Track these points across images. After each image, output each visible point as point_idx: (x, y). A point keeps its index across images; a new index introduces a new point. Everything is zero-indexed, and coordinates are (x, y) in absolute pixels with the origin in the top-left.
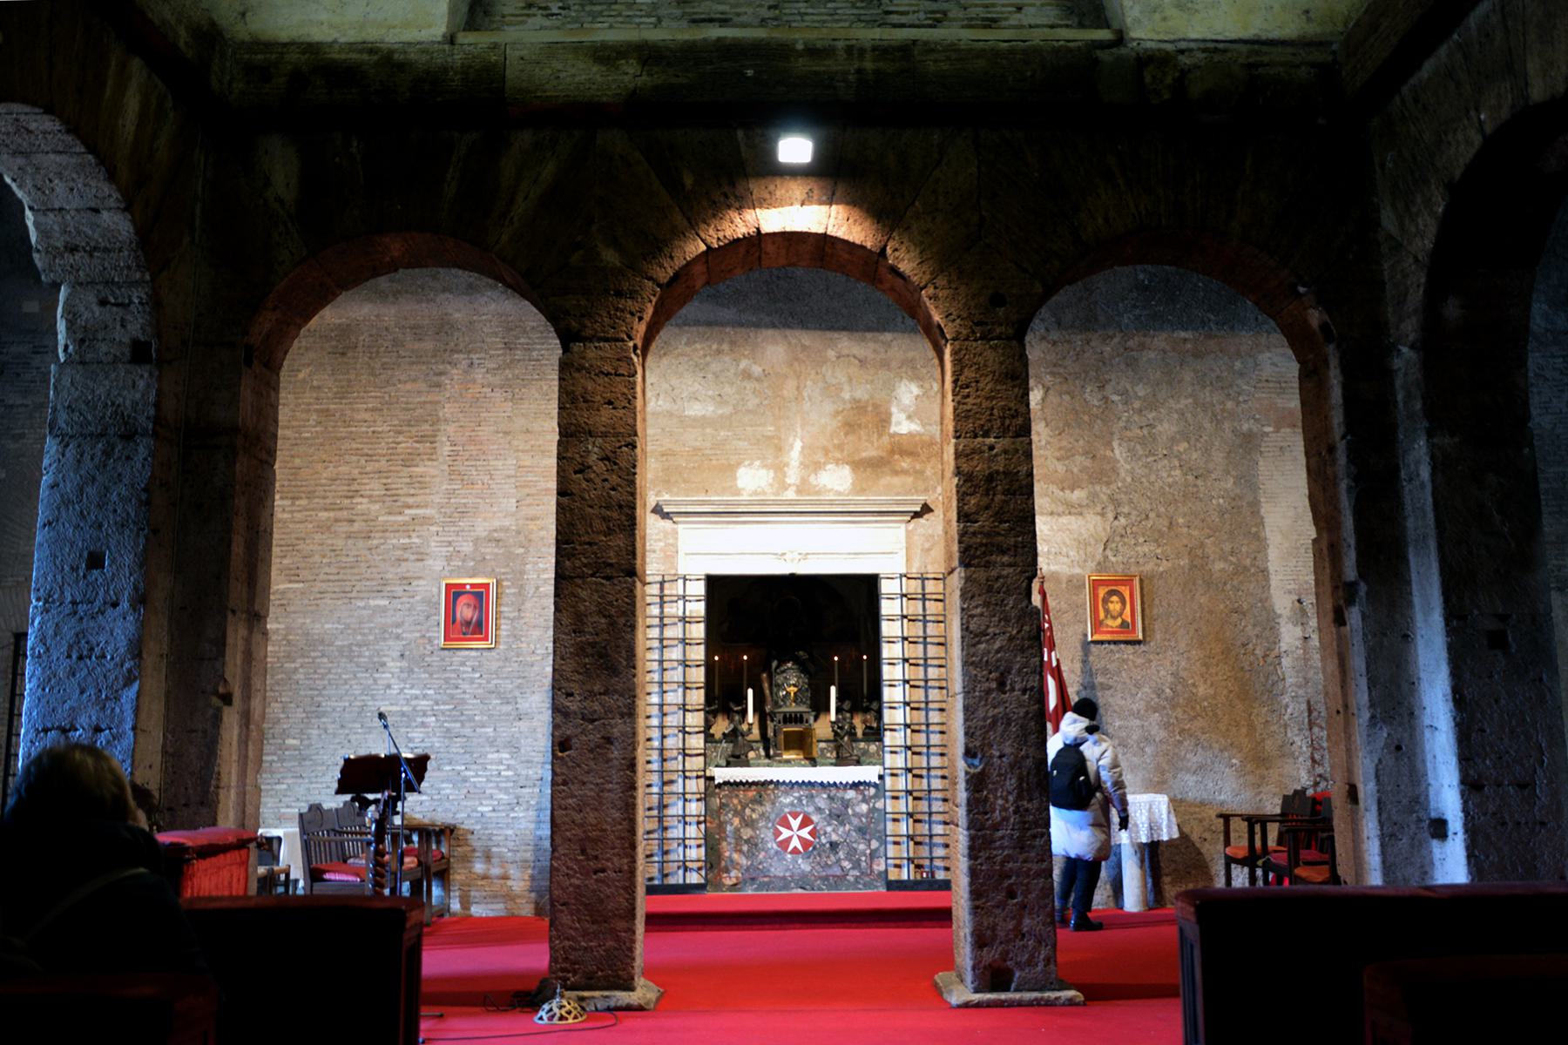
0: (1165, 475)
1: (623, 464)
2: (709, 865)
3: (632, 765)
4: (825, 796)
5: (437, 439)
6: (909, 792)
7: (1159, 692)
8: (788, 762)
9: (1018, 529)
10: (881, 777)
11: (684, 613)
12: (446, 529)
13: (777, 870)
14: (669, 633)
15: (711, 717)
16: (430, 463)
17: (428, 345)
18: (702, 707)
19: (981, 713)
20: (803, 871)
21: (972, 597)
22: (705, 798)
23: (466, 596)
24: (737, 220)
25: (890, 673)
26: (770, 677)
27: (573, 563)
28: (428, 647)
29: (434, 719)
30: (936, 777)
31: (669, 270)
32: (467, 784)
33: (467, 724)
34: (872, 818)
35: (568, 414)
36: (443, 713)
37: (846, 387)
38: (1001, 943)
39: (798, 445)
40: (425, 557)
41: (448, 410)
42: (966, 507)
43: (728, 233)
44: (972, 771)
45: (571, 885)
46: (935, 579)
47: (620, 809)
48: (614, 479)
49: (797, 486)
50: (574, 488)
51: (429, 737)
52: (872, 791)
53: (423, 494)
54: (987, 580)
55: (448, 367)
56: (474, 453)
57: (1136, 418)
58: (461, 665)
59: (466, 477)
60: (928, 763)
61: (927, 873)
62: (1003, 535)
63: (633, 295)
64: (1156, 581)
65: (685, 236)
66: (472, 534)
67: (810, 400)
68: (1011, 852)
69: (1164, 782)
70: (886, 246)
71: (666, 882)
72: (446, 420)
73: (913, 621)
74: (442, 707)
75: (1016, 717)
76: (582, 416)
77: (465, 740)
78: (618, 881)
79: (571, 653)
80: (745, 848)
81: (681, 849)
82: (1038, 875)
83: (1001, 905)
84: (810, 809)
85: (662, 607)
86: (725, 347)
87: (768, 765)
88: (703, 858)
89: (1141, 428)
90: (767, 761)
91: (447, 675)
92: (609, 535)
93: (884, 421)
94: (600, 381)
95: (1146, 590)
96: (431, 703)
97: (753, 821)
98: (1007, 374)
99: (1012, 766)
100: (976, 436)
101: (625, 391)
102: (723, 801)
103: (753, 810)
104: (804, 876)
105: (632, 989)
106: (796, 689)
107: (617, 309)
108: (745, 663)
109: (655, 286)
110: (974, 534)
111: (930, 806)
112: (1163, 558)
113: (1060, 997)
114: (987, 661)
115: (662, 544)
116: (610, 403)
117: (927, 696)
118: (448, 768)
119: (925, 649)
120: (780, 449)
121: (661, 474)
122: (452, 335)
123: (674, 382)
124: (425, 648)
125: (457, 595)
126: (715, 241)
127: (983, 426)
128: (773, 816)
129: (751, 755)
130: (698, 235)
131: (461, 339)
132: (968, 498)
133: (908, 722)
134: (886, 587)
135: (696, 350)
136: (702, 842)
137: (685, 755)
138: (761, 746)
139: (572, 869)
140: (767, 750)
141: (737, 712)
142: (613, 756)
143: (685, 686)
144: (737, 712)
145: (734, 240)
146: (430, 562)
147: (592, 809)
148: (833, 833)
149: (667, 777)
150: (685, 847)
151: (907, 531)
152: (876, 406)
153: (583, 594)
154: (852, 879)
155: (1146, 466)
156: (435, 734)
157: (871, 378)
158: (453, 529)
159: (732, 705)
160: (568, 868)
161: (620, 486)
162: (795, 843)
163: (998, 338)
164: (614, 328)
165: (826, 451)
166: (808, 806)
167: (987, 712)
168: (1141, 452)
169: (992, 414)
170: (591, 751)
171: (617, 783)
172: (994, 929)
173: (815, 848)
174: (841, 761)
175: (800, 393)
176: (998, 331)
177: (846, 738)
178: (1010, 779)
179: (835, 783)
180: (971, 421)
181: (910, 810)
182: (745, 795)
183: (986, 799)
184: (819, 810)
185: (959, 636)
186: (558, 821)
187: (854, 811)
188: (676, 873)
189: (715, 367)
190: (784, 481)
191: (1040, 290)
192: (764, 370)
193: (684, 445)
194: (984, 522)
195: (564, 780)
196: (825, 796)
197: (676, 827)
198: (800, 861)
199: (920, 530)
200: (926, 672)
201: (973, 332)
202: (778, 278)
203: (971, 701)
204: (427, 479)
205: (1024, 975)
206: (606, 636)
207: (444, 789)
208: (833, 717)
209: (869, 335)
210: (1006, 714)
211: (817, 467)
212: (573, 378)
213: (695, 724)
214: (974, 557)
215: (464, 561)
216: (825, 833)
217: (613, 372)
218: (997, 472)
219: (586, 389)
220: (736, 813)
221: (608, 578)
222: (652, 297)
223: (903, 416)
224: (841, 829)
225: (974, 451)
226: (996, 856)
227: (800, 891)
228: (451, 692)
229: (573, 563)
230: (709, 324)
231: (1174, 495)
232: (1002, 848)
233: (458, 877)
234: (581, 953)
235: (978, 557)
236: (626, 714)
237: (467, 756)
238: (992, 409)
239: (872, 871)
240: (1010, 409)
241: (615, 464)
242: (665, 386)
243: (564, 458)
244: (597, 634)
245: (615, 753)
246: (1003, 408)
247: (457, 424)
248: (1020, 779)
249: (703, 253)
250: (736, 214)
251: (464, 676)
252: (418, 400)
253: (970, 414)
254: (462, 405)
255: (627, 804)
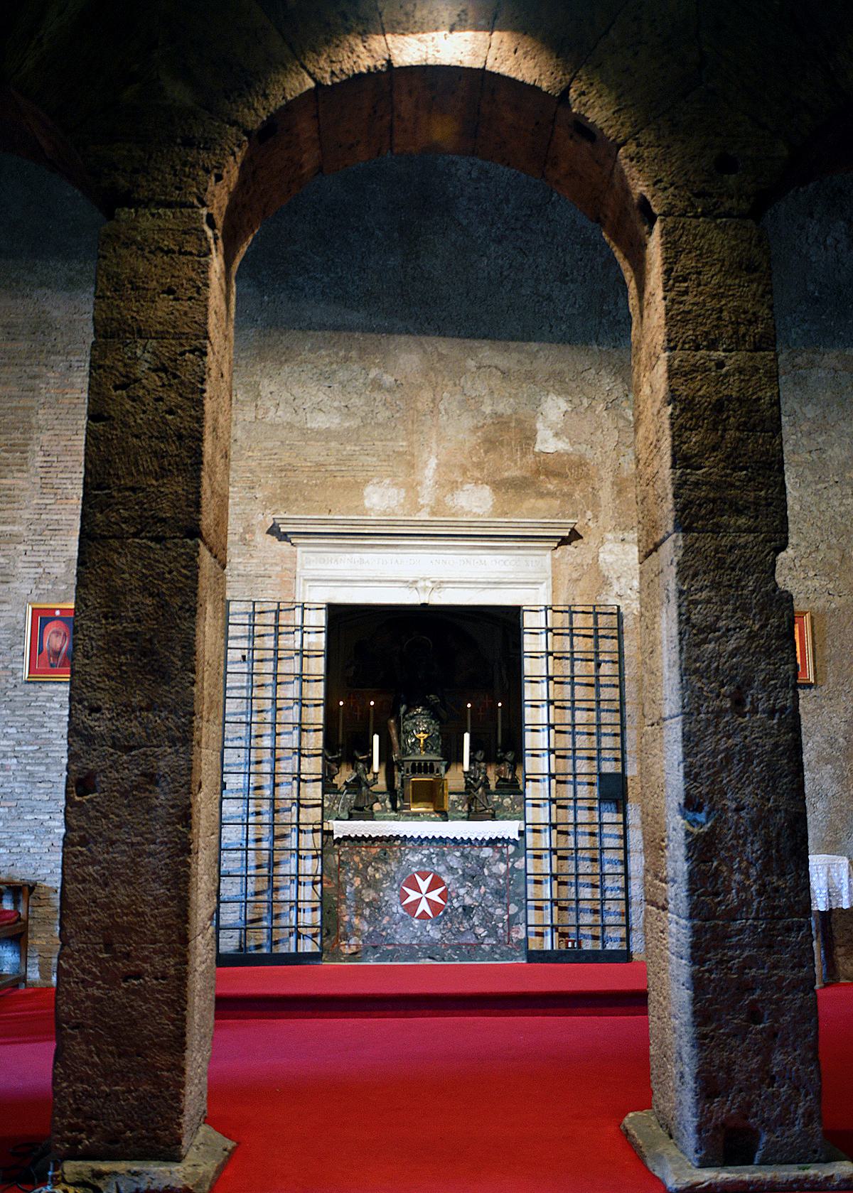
0: (837, 503)
1: (186, 377)
2: (325, 932)
3: (185, 816)
4: (458, 854)
5: (28, 448)
6: (553, 851)
7: (832, 742)
8: (416, 815)
9: (761, 479)
10: (521, 833)
11: (302, 645)
12: (35, 548)
13: (403, 937)
14: (283, 667)
15: (334, 767)
16: (19, 475)
17: (23, 345)
18: (320, 752)
19: (709, 745)
20: (432, 938)
21: (695, 575)
22: (321, 854)
23: (55, 623)
24: (360, 48)
25: (534, 717)
26: (398, 722)
27: (107, 517)
28: (11, 680)
29: (15, 761)
30: (584, 834)
31: (261, 112)
32: (51, 836)
33: (53, 768)
34: (511, 879)
35: (108, 306)
36: (26, 754)
37: (487, 401)
38: (741, 1090)
39: (433, 462)
40: (11, 579)
41: (42, 416)
42: (684, 447)
43: (347, 66)
44: (696, 830)
45: (88, 997)
46: (583, 612)
47: (166, 883)
48: (173, 398)
49: (432, 508)
50: (114, 410)
51: (9, 782)
52: (511, 849)
53: (10, 509)
54: (717, 551)
55: (44, 370)
56: (70, 464)
57: (804, 441)
58: (47, 701)
59: (60, 491)
60: (575, 819)
61: (573, 942)
62: (737, 488)
63: (208, 144)
64: (827, 619)
65: (286, 68)
66: (65, 554)
67: (447, 413)
68: (754, 952)
69: (837, 842)
70: (568, 88)
71: (275, 951)
72: (39, 428)
73: (560, 658)
74: (25, 748)
75: (760, 750)
76: (129, 309)
77: (50, 785)
78: (159, 992)
79: (99, 648)
80: (367, 912)
81: (293, 913)
82: (794, 986)
83: (740, 1033)
84: (441, 869)
85: (276, 640)
86: (354, 354)
87: (395, 819)
88: (319, 924)
89: (810, 452)
90: (393, 814)
91: (31, 712)
92: (163, 477)
93: (529, 438)
94: (158, 261)
95: (816, 629)
96: (12, 743)
97: (376, 881)
98: (740, 264)
99: (755, 824)
100: (697, 348)
101: (193, 275)
102: (342, 858)
103: (377, 870)
104: (433, 944)
105: (178, 1159)
106: (426, 736)
107: (185, 164)
108: (371, 710)
109: (240, 134)
110: (696, 484)
111: (577, 867)
112: (835, 593)
113: (831, 1178)
114: (717, 668)
115: (279, 569)
116: (170, 291)
117: (574, 743)
118: (29, 817)
119: (573, 689)
120: (413, 467)
121: (279, 491)
122: (49, 335)
123: (296, 390)
124: (7, 681)
125: (45, 622)
126: (327, 76)
127: (707, 333)
128: (399, 876)
129: (377, 807)
130: (304, 67)
131: (59, 340)
132: (688, 433)
133: (553, 771)
134: (529, 620)
135: (321, 357)
136: (318, 904)
137: (300, 806)
138: (387, 797)
139: (90, 973)
140: (393, 802)
141: (362, 761)
142: (157, 802)
143: (302, 728)
144: (362, 761)
145: (355, 75)
146: (17, 585)
147: (123, 882)
148: (467, 896)
149: (278, 831)
150: (298, 910)
151: (553, 559)
152: (519, 421)
153: (121, 562)
154: (487, 948)
155: (816, 493)
156: (15, 778)
157: (514, 391)
158: (42, 548)
159: (356, 754)
160: (83, 970)
161: (180, 407)
162: (424, 906)
163: (728, 215)
164: (180, 189)
165: (464, 470)
166: (438, 865)
167: (717, 743)
168: (810, 478)
169: (719, 318)
170: (125, 794)
171: (162, 843)
172: (729, 1070)
173: (446, 913)
174: (472, 816)
175: (436, 406)
176: (727, 205)
177: (480, 790)
178: (752, 843)
179: (469, 839)
180: (690, 326)
181: (555, 871)
182: (367, 852)
183: (717, 872)
184: (451, 870)
185: (675, 631)
186: (72, 900)
187: (490, 870)
188: (288, 940)
189: (342, 375)
190: (417, 503)
191: (786, 153)
192: (396, 380)
193: (305, 460)
194: (710, 468)
195: (82, 837)
196: (458, 854)
197: (289, 888)
198: (429, 927)
199: (568, 559)
200: (573, 716)
201: (692, 205)
202: (414, 278)
203: (694, 727)
204: (17, 492)
205: (773, 1139)
206: (153, 624)
207: (24, 841)
208: (466, 767)
209: (513, 345)
210: (745, 747)
211: (454, 486)
212: (120, 256)
213: (312, 771)
214: (697, 517)
215: (54, 584)
216: (458, 896)
217: (177, 248)
218: (729, 398)
219: (136, 272)
220: (358, 872)
221: (158, 539)
222: (236, 149)
223: (550, 433)
224: (476, 892)
225: (695, 369)
226: (733, 958)
227: (428, 962)
228: (35, 731)
229: (107, 517)
230: (336, 328)
231: (846, 526)
232: (742, 947)
233: (38, 942)
234: (100, 1102)
235: (702, 518)
236: (178, 738)
237: (53, 804)
238: (721, 311)
239: (510, 939)
240: (745, 312)
241: (175, 376)
242: (286, 395)
243: (100, 367)
244: (139, 621)
245: (161, 798)
246: (735, 310)
247: (51, 432)
248: (767, 844)
249: (310, 90)
250: (359, 42)
251: (51, 713)
252: (9, 405)
253: (689, 317)
254: (59, 411)
255: (177, 875)
